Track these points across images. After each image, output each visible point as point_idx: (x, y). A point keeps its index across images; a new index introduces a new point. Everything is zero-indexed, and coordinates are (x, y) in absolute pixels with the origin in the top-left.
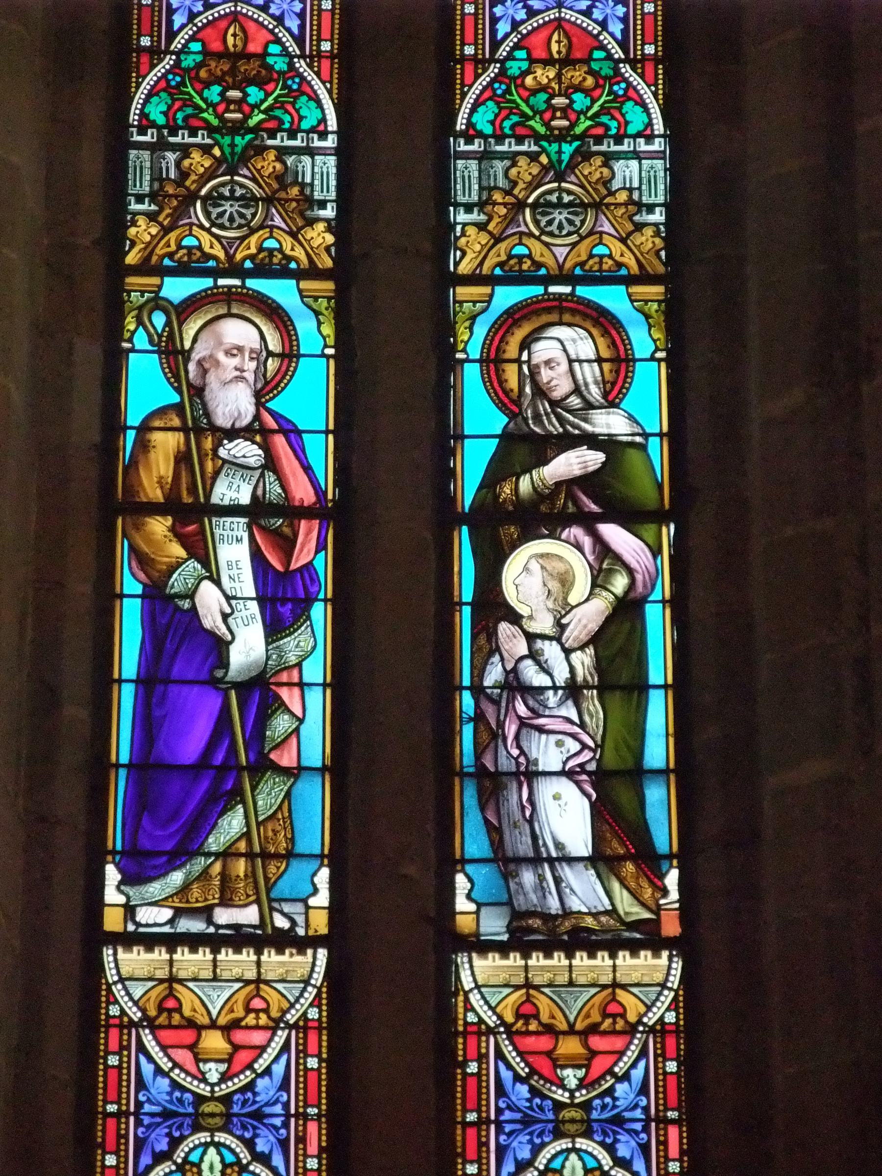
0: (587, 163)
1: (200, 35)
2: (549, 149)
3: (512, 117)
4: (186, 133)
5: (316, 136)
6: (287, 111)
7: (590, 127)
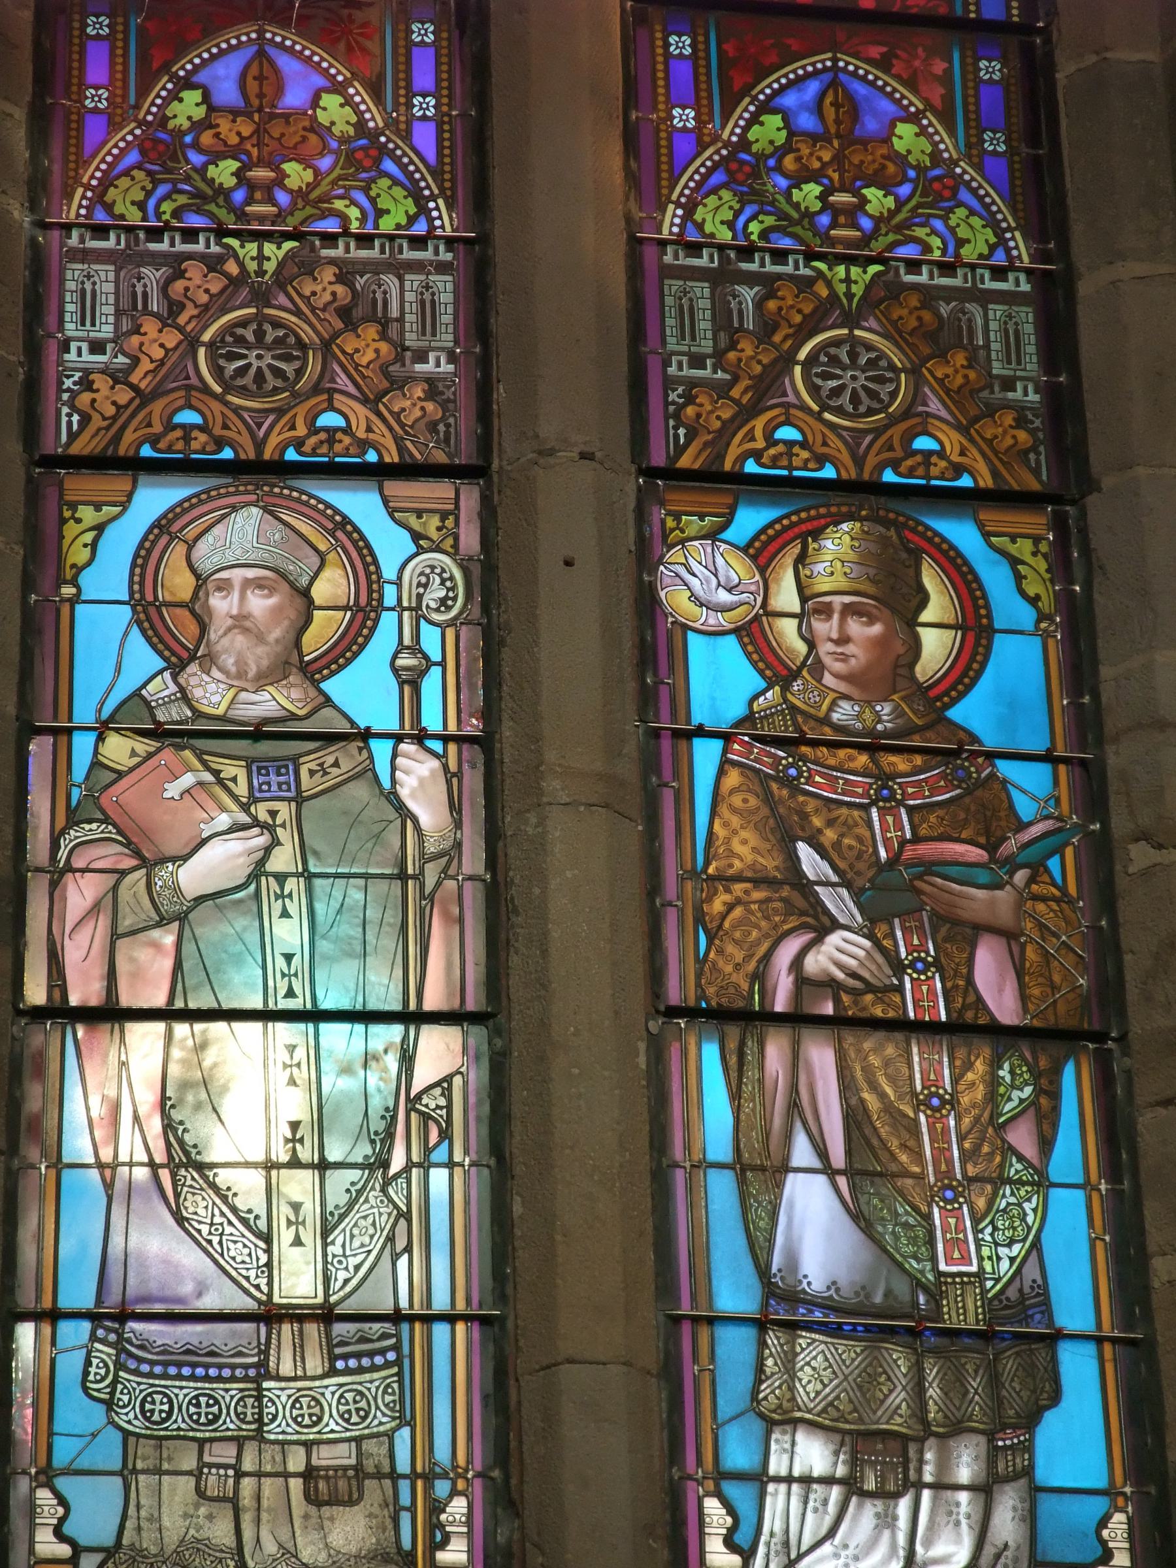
1: (201, 77)
2: (241, 252)
3: (174, 196)
6: (354, 203)
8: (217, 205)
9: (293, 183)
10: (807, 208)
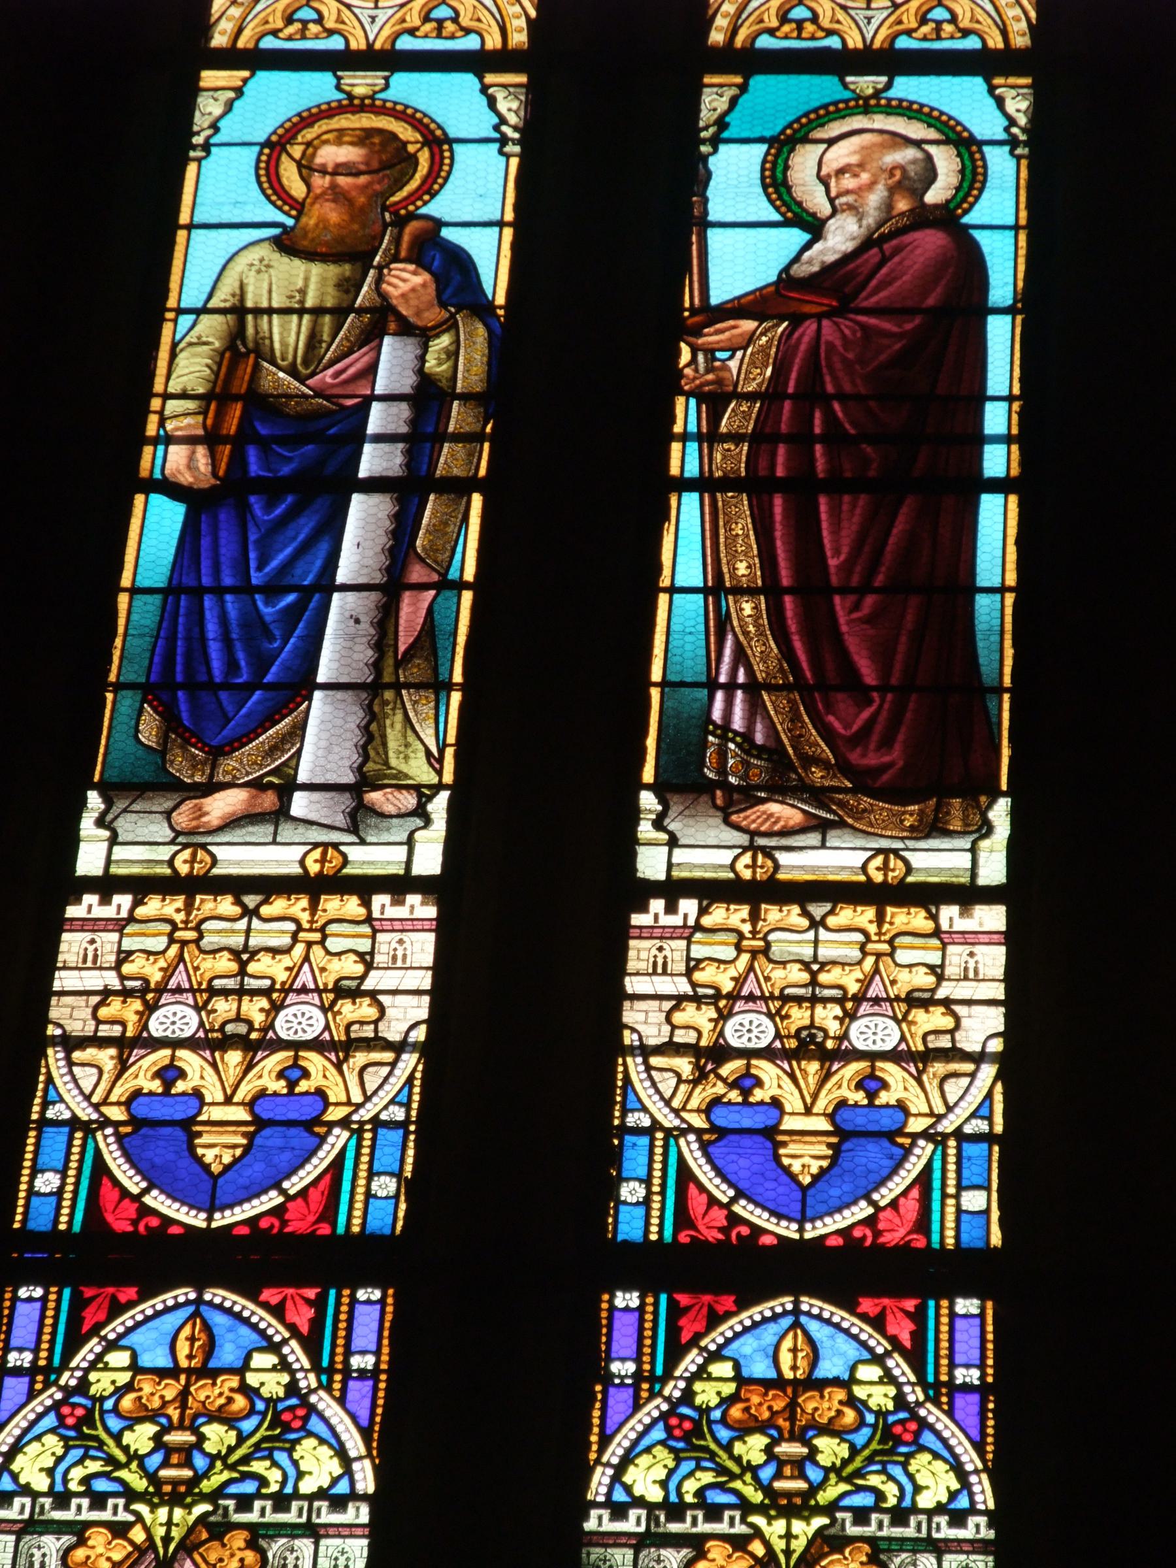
0: (216, 1544)
2: (148, 1517)
3: (698, 1474)
4: (700, 1515)
5: (324, 1505)
7: (231, 1481)
8: (744, 1483)
9: (824, 1459)
10: (749, 1462)
